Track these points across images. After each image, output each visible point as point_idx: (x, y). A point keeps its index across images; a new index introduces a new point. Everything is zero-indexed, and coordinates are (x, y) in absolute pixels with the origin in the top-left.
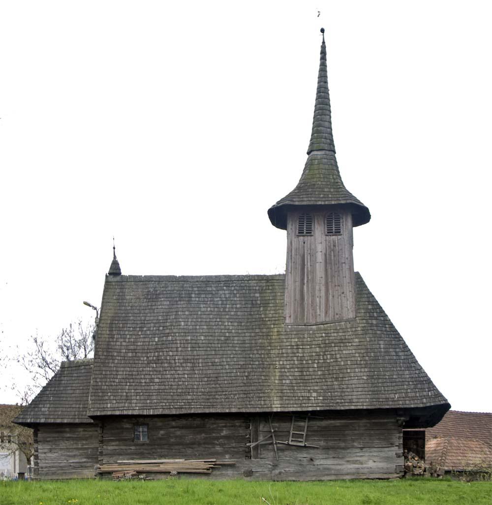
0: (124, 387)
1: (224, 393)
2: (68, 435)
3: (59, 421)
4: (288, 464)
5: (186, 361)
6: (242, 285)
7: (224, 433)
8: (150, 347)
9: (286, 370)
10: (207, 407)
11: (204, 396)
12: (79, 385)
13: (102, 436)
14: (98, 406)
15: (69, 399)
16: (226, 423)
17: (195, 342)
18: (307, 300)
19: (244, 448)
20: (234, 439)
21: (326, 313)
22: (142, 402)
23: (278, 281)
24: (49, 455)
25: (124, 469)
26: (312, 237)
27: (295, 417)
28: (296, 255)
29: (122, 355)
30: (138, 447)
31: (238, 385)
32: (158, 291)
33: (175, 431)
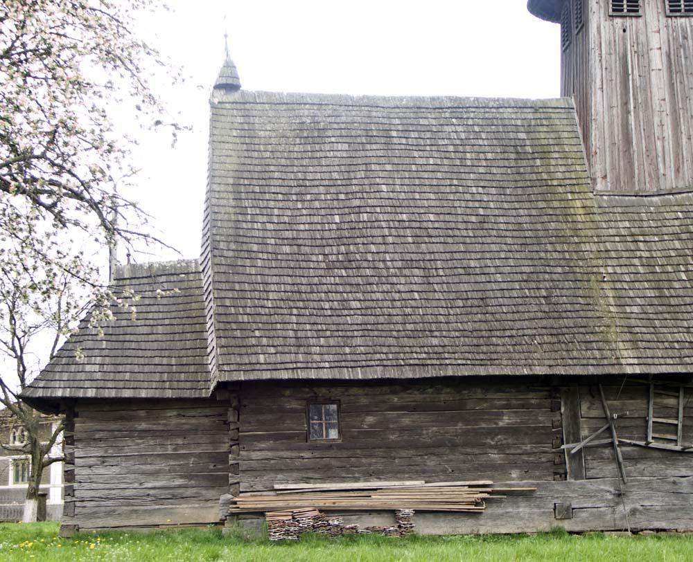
0: (287, 318)
1: (508, 333)
2: (144, 426)
3: (127, 394)
4: (649, 494)
5: (409, 264)
6: (487, 115)
7: (506, 420)
8: (327, 234)
9: (625, 286)
10: (478, 362)
11: (466, 339)
12: (161, 316)
13: (238, 429)
14: (238, 360)
15: (143, 345)
16: (507, 400)
17: (418, 225)
18: (637, 144)
19: (550, 456)
20: (526, 434)
21: (678, 171)
22: (333, 350)
23: (557, 110)
24: (101, 471)
25: (291, 504)
26: (640, 20)
27: (656, 387)
28: (610, 54)
29: (270, 249)
30: (317, 454)
31: (531, 315)
32: (322, 124)
33: (399, 416)
